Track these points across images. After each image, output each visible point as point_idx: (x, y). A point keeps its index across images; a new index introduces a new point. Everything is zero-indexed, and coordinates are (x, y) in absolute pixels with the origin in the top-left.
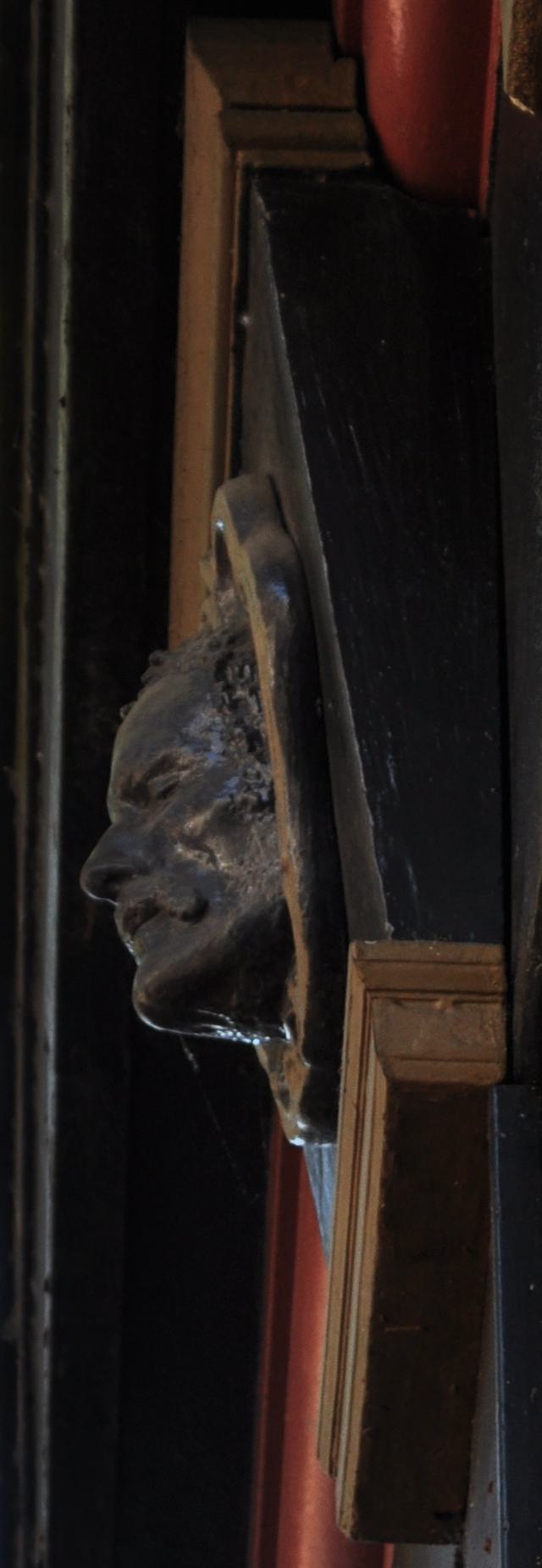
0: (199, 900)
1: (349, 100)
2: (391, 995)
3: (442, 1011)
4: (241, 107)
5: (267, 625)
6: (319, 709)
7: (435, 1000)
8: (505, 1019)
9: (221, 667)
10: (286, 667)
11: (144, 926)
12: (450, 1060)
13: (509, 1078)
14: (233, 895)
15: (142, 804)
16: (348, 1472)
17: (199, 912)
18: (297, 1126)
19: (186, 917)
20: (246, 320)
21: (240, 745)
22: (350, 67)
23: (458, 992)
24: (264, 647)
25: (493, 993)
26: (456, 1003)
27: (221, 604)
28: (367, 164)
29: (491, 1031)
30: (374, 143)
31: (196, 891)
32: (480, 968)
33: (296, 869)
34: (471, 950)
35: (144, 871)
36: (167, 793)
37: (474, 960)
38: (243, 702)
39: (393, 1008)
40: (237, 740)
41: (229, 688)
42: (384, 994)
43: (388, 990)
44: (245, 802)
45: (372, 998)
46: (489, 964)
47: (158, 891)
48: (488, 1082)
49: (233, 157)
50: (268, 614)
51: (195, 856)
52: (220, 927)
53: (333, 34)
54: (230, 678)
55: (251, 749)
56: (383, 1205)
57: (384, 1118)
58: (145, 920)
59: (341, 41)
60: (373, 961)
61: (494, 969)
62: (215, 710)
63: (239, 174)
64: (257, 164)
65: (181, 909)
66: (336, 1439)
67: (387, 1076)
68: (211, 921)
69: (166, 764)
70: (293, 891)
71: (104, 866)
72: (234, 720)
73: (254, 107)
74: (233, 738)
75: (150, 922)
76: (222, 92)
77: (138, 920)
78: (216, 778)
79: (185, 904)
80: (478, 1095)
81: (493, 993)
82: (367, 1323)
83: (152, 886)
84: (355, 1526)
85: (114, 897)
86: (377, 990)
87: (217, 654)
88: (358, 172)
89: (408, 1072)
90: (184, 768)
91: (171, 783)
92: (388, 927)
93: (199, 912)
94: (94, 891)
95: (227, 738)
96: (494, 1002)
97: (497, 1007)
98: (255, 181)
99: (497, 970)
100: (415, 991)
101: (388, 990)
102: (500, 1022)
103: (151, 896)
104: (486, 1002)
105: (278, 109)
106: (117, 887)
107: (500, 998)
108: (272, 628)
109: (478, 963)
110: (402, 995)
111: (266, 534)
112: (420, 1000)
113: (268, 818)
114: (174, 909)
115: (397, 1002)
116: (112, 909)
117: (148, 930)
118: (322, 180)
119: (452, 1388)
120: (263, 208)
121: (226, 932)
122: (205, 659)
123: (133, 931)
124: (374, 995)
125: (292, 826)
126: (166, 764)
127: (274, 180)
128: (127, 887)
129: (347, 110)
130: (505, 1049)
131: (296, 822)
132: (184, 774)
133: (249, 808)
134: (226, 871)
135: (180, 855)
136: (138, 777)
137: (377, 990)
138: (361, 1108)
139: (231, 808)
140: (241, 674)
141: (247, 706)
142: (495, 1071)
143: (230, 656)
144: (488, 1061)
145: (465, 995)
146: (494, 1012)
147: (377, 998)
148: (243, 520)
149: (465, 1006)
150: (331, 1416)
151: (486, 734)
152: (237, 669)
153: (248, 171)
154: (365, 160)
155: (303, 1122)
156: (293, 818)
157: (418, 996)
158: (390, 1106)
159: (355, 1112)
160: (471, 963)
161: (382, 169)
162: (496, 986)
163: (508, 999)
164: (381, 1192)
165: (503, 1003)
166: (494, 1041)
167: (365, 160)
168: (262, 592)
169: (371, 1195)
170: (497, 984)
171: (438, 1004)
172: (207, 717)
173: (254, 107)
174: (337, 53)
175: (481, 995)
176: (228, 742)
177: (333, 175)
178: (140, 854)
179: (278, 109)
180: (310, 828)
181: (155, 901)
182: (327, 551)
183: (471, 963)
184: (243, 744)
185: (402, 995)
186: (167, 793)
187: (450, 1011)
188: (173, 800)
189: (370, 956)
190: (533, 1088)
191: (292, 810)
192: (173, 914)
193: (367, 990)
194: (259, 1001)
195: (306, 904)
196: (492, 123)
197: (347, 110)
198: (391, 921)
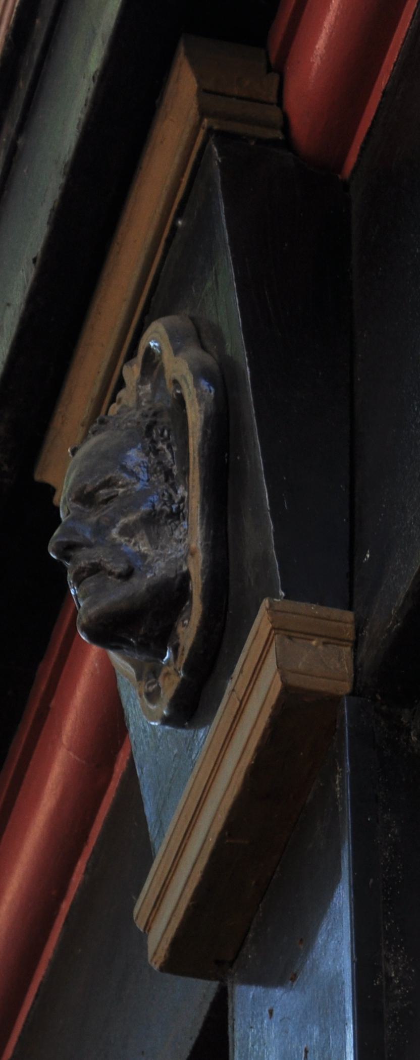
0: (129, 567)
1: (273, 98)
2: (287, 633)
3: (317, 646)
4: (205, 91)
5: (200, 405)
6: (226, 460)
7: (312, 640)
8: (353, 657)
9: (150, 428)
10: (209, 431)
11: (88, 579)
12: (320, 677)
13: (353, 693)
14: (150, 567)
15: (87, 506)
16: (170, 927)
17: (127, 575)
18: (163, 712)
19: (120, 576)
20: (180, 223)
21: (160, 478)
22: (276, 78)
23: (325, 636)
24: (195, 417)
25: (348, 641)
26: (325, 643)
27: (141, 393)
28: (281, 138)
29: (345, 663)
30: (286, 126)
31: (128, 561)
32: (341, 624)
33: (200, 556)
34: (336, 613)
35: (90, 546)
36: (106, 501)
37: (338, 619)
38: (162, 452)
39: (287, 641)
40: (158, 474)
41: (154, 442)
42: (282, 632)
43: (286, 630)
44: (162, 511)
45: (275, 634)
46: (346, 622)
47: (103, 559)
48: (341, 693)
49: (201, 121)
50: (200, 398)
51: (125, 541)
52: (140, 584)
53: (268, 57)
54: (155, 436)
55: (167, 480)
56: (253, 762)
57: (272, 708)
58: (89, 575)
59: (273, 61)
60: (278, 611)
61: (349, 626)
62: (144, 455)
63: (202, 132)
64: (216, 127)
65: (117, 571)
66: (156, 909)
67: (282, 681)
68: (135, 580)
69: (109, 484)
70: (196, 568)
71: (65, 539)
72: (156, 461)
73: (216, 93)
74: (155, 472)
75: (92, 577)
76: (198, 82)
77: (85, 575)
78: (144, 493)
79: (120, 568)
80: (333, 701)
81: (348, 641)
82: (216, 835)
83: (99, 555)
84: (164, 962)
85: (68, 559)
86: (278, 629)
87: (148, 420)
88: (275, 142)
89: (294, 680)
90: (122, 486)
91: (113, 494)
92: (282, 594)
93: (127, 575)
94: (56, 553)
95: (150, 471)
96: (346, 646)
97: (348, 649)
98: (212, 138)
99: (350, 627)
100: (301, 633)
101: (286, 630)
102: (350, 658)
103: (97, 561)
104: (342, 645)
105: (231, 96)
106: (72, 553)
107: (351, 644)
108: (203, 405)
109: (340, 621)
110: (292, 634)
111: (194, 352)
112: (303, 638)
113: (177, 522)
114: (113, 570)
115: (290, 637)
116: (65, 569)
117: (91, 583)
118: (253, 143)
119: (254, 882)
120: (217, 155)
121: (144, 588)
122: (139, 423)
123: (79, 582)
124: (276, 631)
125: (201, 528)
126: (109, 484)
127: (223, 137)
128: (79, 554)
129: (272, 104)
130: (353, 675)
131: (204, 527)
132: (121, 490)
133: (164, 515)
134: (146, 552)
135: (114, 539)
136: (89, 489)
137: (278, 629)
138: (244, 703)
139: (153, 514)
140: (162, 435)
141: (164, 455)
142: (346, 687)
143: (155, 423)
144: (343, 681)
145: (331, 639)
146: (347, 650)
147: (278, 634)
148: (177, 340)
149: (329, 646)
150: (157, 894)
151: (341, 486)
152: (159, 432)
153: (210, 131)
154: (279, 135)
155: (166, 711)
156: (202, 524)
157: (302, 636)
158: (279, 700)
159: (238, 703)
160: (335, 621)
161: (288, 143)
162: (350, 636)
163: (356, 645)
164: (254, 755)
165: (352, 647)
166: (347, 669)
167: (279, 135)
168: (196, 385)
169: (245, 754)
170: (350, 634)
171: (314, 643)
172: (135, 456)
173: (216, 93)
174: (269, 69)
175: (340, 641)
176: (152, 475)
177: (260, 141)
178: (88, 535)
179: (231, 96)
180: (212, 531)
181: (100, 564)
182: (251, 364)
183: (335, 621)
184: (162, 477)
185: (292, 634)
186: (106, 501)
187: (321, 647)
188: (113, 505)
189: (276, 608)
190: (369, 701)
191: (202, 519)
192: (111, 573)
193: (273, 628)
194: (156, 634)
195: (204, 577)
196: (369, 124)
197: (272, 104)
198: (284, 590)
